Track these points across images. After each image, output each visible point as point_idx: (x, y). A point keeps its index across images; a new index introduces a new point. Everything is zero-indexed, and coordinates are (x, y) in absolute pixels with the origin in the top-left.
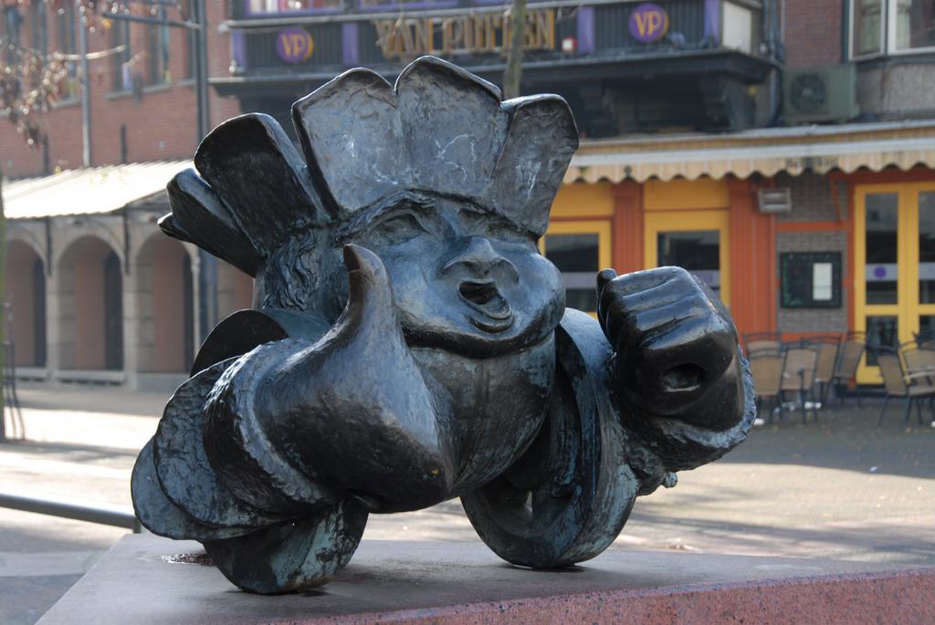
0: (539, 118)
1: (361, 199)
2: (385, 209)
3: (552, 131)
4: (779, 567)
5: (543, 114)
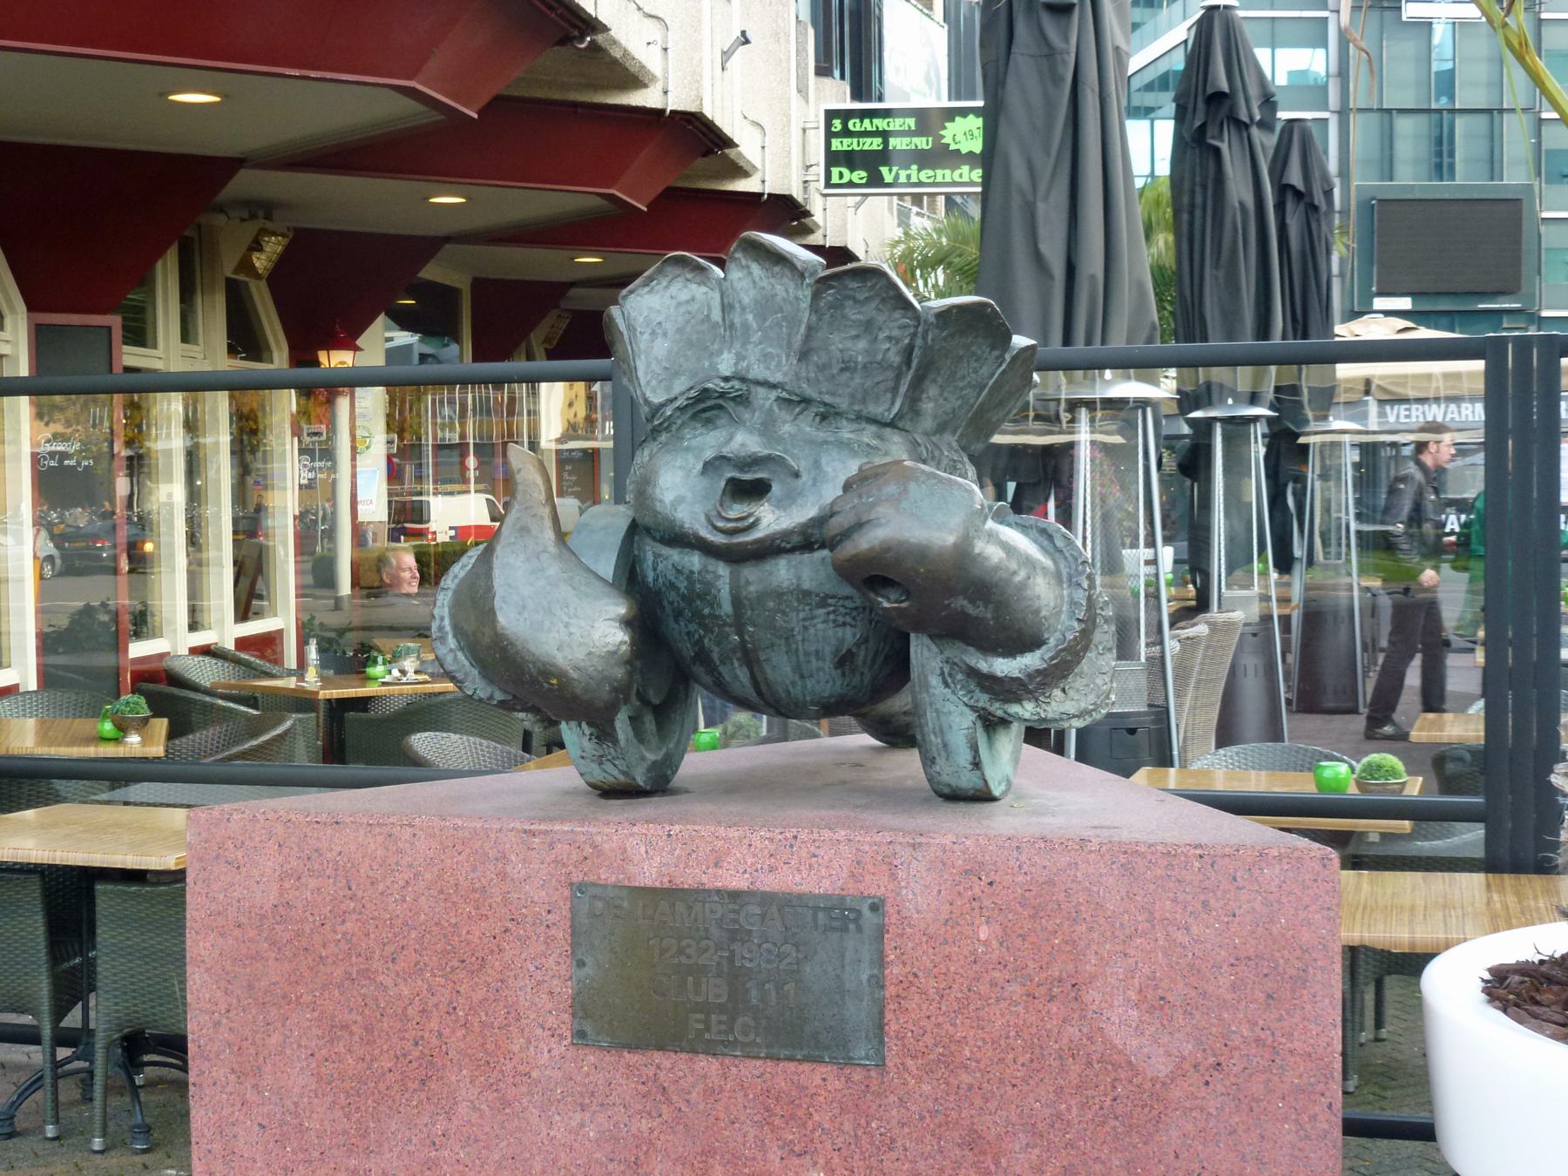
3: (873, 305)
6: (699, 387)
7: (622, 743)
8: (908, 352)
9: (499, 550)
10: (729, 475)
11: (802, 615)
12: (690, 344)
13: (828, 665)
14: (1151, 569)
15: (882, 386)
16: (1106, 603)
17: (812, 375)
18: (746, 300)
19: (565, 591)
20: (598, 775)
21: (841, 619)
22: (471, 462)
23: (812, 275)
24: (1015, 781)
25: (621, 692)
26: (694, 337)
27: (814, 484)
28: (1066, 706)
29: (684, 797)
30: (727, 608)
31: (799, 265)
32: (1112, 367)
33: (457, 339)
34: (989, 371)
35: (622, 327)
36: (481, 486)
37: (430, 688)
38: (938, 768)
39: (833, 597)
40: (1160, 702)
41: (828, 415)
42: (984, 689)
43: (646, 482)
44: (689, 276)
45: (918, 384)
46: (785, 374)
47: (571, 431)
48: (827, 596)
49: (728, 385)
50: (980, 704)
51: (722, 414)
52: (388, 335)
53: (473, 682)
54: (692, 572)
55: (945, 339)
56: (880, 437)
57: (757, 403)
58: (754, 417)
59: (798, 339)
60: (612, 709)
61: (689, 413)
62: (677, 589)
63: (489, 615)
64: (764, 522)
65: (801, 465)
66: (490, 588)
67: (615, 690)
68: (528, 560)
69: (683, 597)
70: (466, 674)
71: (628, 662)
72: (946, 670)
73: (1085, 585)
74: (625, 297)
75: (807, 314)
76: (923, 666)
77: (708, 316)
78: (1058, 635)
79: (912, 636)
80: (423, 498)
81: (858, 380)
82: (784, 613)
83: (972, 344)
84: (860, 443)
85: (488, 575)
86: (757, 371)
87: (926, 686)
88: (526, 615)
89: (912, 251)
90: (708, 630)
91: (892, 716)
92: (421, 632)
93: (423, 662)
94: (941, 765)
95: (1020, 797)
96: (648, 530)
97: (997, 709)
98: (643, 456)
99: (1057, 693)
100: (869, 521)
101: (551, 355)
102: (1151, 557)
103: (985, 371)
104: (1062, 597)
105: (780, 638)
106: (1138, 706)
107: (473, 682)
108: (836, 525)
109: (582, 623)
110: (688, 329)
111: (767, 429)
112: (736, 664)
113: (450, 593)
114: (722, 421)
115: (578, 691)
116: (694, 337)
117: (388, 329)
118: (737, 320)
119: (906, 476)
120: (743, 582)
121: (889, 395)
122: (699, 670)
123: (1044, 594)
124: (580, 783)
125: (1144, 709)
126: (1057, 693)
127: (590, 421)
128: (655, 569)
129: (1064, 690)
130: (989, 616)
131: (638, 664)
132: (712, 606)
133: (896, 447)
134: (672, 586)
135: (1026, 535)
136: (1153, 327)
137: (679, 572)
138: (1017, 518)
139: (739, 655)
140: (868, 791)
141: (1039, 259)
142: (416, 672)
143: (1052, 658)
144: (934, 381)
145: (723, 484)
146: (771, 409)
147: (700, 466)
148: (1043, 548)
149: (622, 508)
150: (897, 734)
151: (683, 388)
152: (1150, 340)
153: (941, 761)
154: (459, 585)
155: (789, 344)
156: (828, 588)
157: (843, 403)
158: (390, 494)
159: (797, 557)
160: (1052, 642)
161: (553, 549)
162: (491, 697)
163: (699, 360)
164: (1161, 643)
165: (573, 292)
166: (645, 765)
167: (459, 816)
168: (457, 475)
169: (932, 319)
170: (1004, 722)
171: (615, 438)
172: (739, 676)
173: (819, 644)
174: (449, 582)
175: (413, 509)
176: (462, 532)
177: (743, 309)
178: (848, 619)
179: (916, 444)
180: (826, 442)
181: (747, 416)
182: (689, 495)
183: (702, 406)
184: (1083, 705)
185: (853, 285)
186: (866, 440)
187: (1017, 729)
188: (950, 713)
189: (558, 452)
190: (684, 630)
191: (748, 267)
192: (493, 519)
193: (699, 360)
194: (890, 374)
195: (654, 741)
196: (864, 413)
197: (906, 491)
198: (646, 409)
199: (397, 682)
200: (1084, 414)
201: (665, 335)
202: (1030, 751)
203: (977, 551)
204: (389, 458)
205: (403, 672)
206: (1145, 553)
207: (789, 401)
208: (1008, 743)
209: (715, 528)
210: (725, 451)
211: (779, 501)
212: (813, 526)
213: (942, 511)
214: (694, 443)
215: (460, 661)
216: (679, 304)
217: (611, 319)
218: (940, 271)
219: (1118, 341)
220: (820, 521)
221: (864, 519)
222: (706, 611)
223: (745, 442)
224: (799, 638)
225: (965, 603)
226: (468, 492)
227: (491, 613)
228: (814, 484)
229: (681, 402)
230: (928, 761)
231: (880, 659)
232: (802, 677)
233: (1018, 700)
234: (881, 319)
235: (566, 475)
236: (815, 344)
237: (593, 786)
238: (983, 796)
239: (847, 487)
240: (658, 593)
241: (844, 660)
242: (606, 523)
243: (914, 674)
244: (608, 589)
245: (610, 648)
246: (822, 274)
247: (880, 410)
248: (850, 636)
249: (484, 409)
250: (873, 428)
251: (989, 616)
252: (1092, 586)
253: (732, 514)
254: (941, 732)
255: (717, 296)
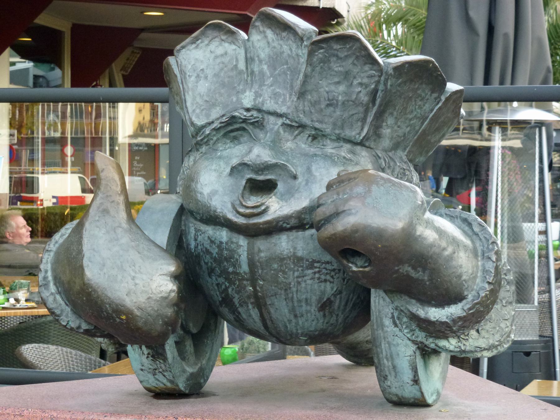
0: (335, 50)
1: (208, 116)
2: (221, 123)
3: (350, 61)
4: (506, 214)
5: (339, 47)
6: (228, 115)
7: (170, 359)
8: (374, 94)
9: (87, 225)
10: (248, 176)
11: (296, 274)
12: (223, 85)
13: (314, 309)
14: (542, 238)
15: (355, 117)
16: (509, 270)
17: (307, 109)
18: (262, 56)
19: (133, 255)
20: (152, 382)
21: (323, 277)
22: (69, 150)
23: (308, 39)
24: (443, 393)
25: (170, 325)
26: (226, 80)
27: (307, 184)
28: (479, 342)
29: (212, 398)
30: (245, 267)
31: (300, 32)
32: (519, 100)
33: (60, 65)
34: (430, 107)
35: (176, 71)
36: (76, 169)
37: (36, 312)
38: (389, 383)
39: (318, 262)
40: (548, 333)
41: (317, 136)
42: (421, 329)
43: (191, 180)
44: (224, 37)
45: (380, 116)
46: (288, 108)
47: (140, 130)
48: (314, 261)
49: (249, 114)
50: (419, 339)
51: (244, 134)
52: (13, 60)
53: (67, 316)
54: (221, 243)
55: (399, 85)
56: (353, 152)
57: (269, 127)
58: (266, 137)
59: (298, 84)
60: (164, 336)
61: (222, 132)
62: (211, 254)
63: (79, 270)
64: (272, 209)
65: (299, 171)
66: (80, 252)
67: (166, 324)
68: (108, 232)
69: (215, 260)
70: (62, 311)
71: (176, 305)
72: (396, 315)
73: (494, 258)
74: (179, 51)
75: (304, 66)
76: (380, 312)
77: (236, 66)
78: (474, 293)
79: (373, 291)
80: (34, 175)
81: (338, 113)
82: (284, 272)
83: (418, 89)
84: (339, 156)
85: (80, 243)
86: (270, 105)
87: (382, 326)
88: (105, 270)
89: (380, 11)
90: (231, 282)
91: (358, 343)
92: (31, 271)
93: (31, 293)
94: (391, 381)
95: (446, 404)
96: (191, 213)
97: (431, 343)
98: (189, 161)
99: (473, 333)
100: (344, 211)
101: (129, 82)
102: (543, 229)
103: (427, 107)
104: (477, 266)
105: (281, 289)
106: (531, 336)
107: (67, 316)
108: (321, 213)
109: (144, 277)
110: (222, 74)
111: (275, 145)
112: (250, 307)
113: (52, 254)
114: (245, 138)
115: (140, 324)
116: (226, 80)
117: (11, 56)
118: (256, 69)
119: (370, 181)
120: (256, 249)
121: (360, 124)
122: (225, 310)
123: (465, 264)
124: (139, 387)
125: (536, 338)
126: (473, 333)
127: (153, 123)
128: (196, 240)
129: (478, 331)
130: (426, 278)
131: (183, 306)
132: (234, 266)
133: (364, 160)
134: (208, 252)
135: (453, 222)
136: (548, 70)
137: (212, 242)
138: (447, 211)
139: (252, 300)
140: (340, 397)
141: (468, 22)
142: (27, 300)
143: (470, 309)
144: (392, 114)
145: (244, 182)
146: (278, 132)
147: (228, 170)
148: (465, 232)
149: (173, 197)
150: (361, 356)
151: (218, 116)
152: (545, 81)
153: (391, 378)
154: (58, 248)
155: (292, 87)
156: (315, 255)
157: (328, 128)
158: (11, 173)
159: (294, 234)
160: (470, 297)
161: (125, 225)
162: (79, 327)
163: (229, 96)
164: (549, 292)
165: (143, 35)
166: (186, 376)
167: (55, 410)
168: (59, 160)
169: (391, 71)
170: (436, 352)
171: (171, 135)
172: (252, 315)
173: (308, 293)
174: (52, 246)
175: (27, 182)
176: (61, 200)
177: (260, 61)
178: (328, 277)
179: (377, 157)
180: (316, 155)
181: (261, 136)
182: (221, 189)
183: (230, 128)
184: (491, 342)
185: (336, 46)
186: (343, 154)
187: (444, 357)
188: (399, 345)
189: (130, 145)
190: (215, 282)
191: (264, 32)
192: (84, 191)
193: (229, 96)
194: (361, 109)
195: (192, 359)
196: (342, 135)
197: (369, 191)
198: (192, 129)
199: (13, 308)
200: (497, 129)
201: (206, 78)
202: (454, 371)
203: (418, 233)
204: (11, 147)
205: (17, 300)
206: (539, 226)
207: (291, 126)
208: (438, 366)
209: (238, 212)
210: (246, 160)
211: (282, 195)
212: (306, 213)
213: (396, 205)
214: (225, 153)
215: (57, 301)
216: (216, 57)
217: (169, 65)
218: (399, 25)
219: (523, 82)
220: (311, 209)
221: (341, 209)
222: (231, 270)
223: (260, 153)
224: (295, 289)
225: (409, 269)
226: (66, 173)
227: (81, 268)
228: (307, 184)
229: (216, 125)
230: (382, 378)
231: (350, 305)
232: (296, 316)
233: (446, 338)
234: (356, 70)
235: (135, 163)
236: (309, 88)
237: (149, 390)
238: (420, 403)
239: (329, 187)
240: (198, 256)
241: (325, 306)
242: (165, 205)
243: (373, 317)
244: (163, 254)
245: (164, 295)
246: (316, 38)
247: (354, 133)
248: (329, 289)
249: (78, 114)
250: (348, 146)
251: (426, 278)
252: (499, 259)
253: (250, 204)
254: (391, 358)
255: (242, 52)
